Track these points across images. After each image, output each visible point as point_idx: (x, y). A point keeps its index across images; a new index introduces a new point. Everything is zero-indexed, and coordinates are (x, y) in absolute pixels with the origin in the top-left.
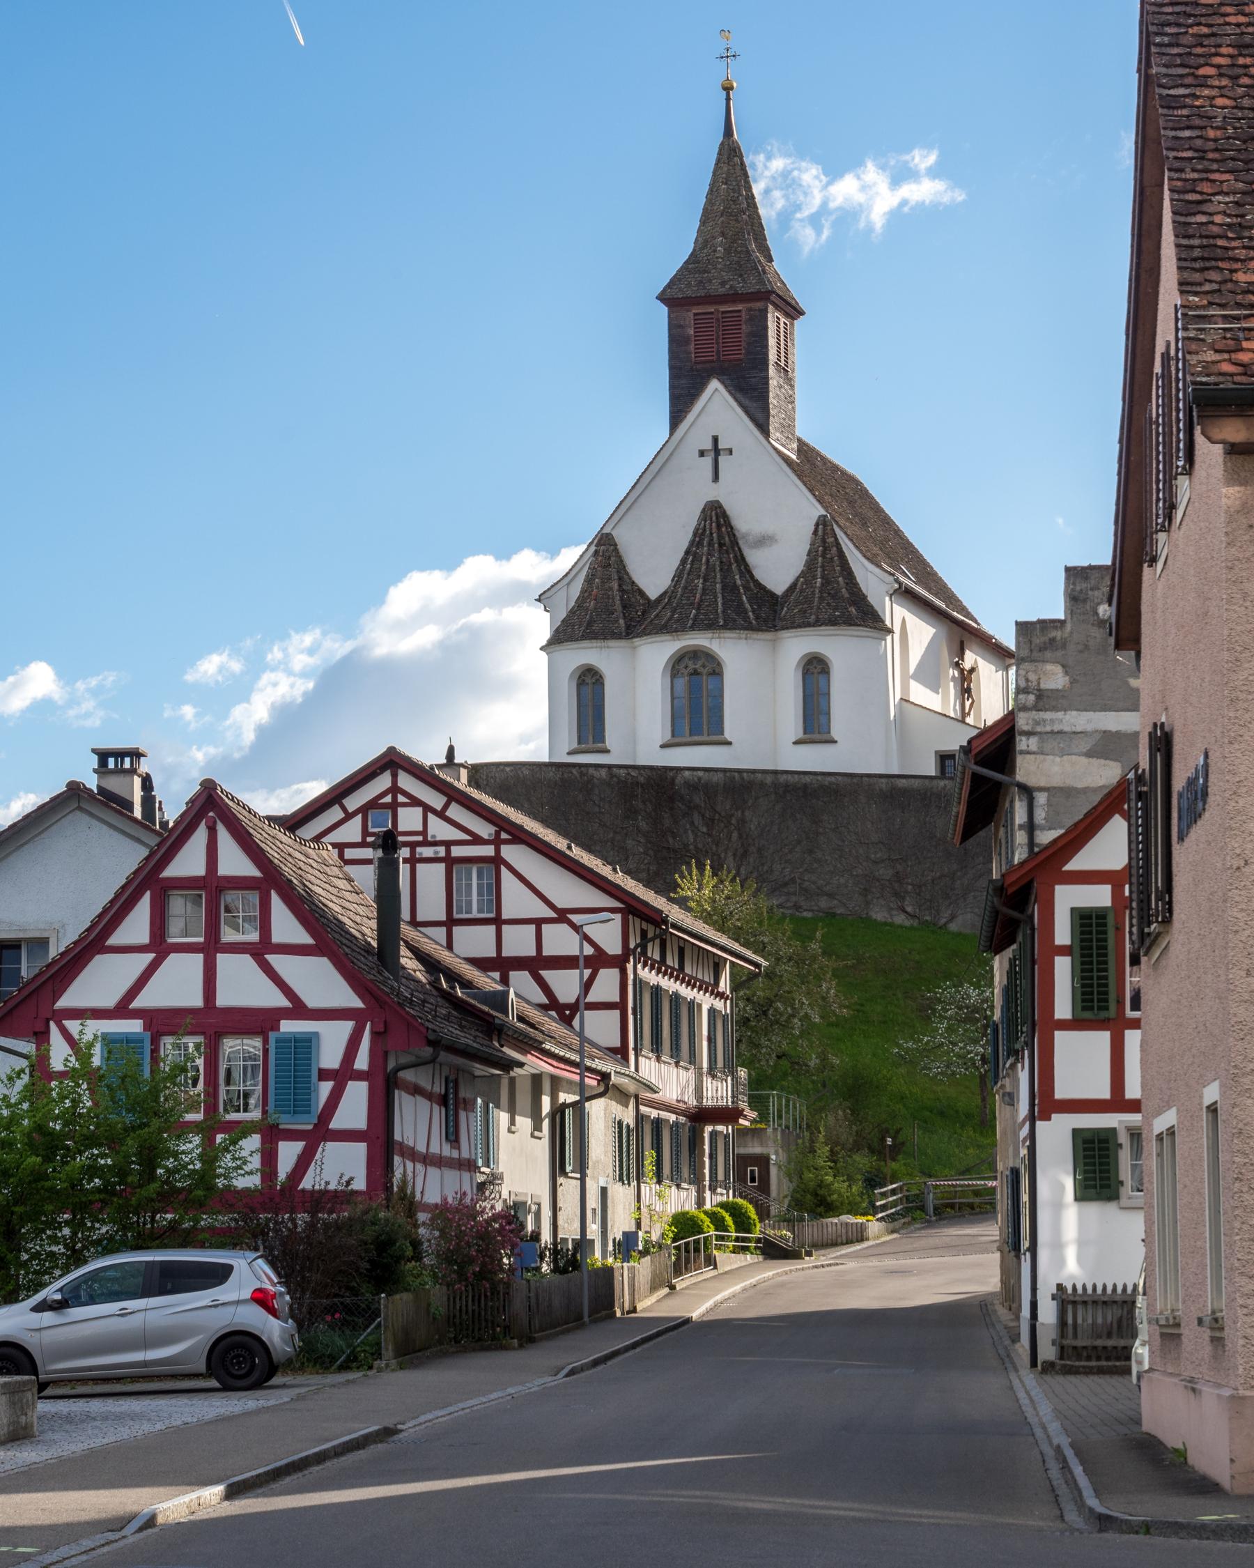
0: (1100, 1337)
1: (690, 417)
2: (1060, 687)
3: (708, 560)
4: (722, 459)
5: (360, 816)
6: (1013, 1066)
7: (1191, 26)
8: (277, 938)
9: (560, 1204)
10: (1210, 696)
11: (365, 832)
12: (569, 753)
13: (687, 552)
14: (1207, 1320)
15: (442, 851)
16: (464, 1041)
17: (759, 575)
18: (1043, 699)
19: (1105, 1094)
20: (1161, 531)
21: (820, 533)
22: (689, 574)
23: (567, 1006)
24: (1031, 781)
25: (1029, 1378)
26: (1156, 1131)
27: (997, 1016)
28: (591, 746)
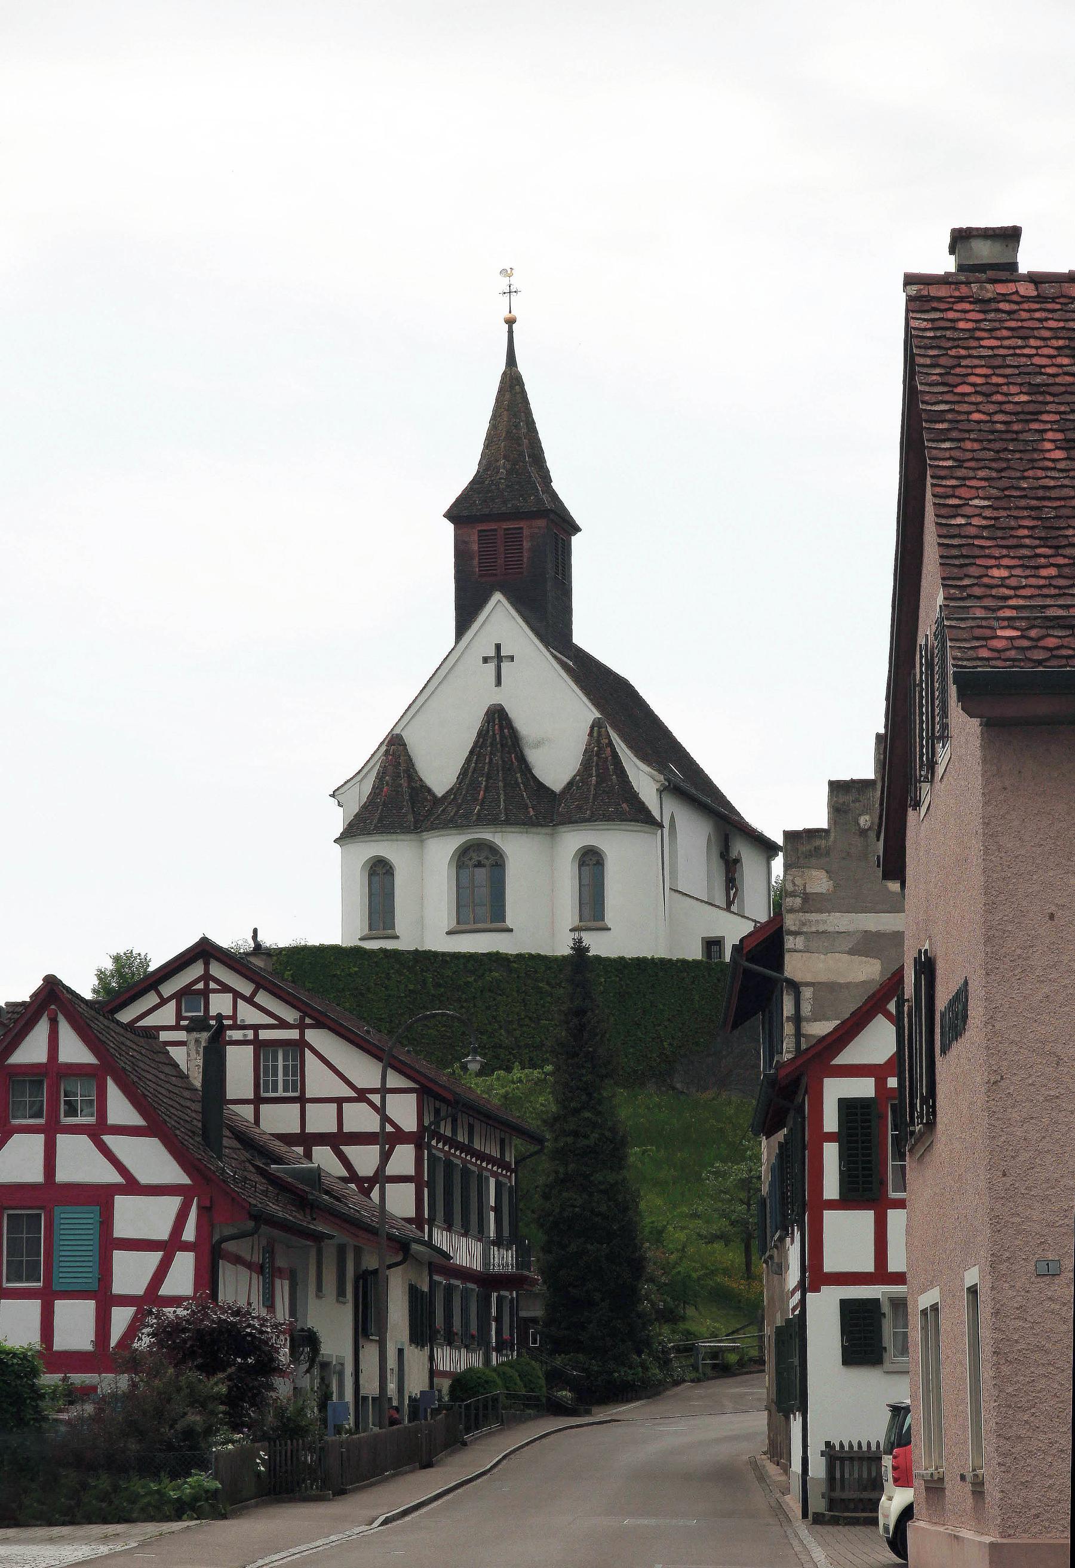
0: (865, 1489)
1: (475, 626)
2: (824, 891)
3: (491, 759)
4: (505, 665)
5: (174, 1002)
6: (782, 1239)
7: (950, 348)
8: (113, 1119)
9: (362, 1366)
10: (970, 932)
11: (179, 1017)
12: (360, 939)
13: (472, 752)
14: (969, 1477)
15: (250, 1035)
16: (280, 1214)
17: (537, 772)
18: (810, 902)
19: (869, 1267)
20: (923, 782)
21: (595, 734)
22: (473, 773)
23: (367, 1179)
24: (798, 977)
25: (802, 1529)
26: (921, 1308)
27: (765, 1189)
28: (381, 933)
